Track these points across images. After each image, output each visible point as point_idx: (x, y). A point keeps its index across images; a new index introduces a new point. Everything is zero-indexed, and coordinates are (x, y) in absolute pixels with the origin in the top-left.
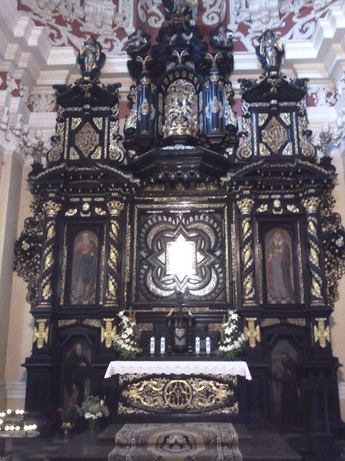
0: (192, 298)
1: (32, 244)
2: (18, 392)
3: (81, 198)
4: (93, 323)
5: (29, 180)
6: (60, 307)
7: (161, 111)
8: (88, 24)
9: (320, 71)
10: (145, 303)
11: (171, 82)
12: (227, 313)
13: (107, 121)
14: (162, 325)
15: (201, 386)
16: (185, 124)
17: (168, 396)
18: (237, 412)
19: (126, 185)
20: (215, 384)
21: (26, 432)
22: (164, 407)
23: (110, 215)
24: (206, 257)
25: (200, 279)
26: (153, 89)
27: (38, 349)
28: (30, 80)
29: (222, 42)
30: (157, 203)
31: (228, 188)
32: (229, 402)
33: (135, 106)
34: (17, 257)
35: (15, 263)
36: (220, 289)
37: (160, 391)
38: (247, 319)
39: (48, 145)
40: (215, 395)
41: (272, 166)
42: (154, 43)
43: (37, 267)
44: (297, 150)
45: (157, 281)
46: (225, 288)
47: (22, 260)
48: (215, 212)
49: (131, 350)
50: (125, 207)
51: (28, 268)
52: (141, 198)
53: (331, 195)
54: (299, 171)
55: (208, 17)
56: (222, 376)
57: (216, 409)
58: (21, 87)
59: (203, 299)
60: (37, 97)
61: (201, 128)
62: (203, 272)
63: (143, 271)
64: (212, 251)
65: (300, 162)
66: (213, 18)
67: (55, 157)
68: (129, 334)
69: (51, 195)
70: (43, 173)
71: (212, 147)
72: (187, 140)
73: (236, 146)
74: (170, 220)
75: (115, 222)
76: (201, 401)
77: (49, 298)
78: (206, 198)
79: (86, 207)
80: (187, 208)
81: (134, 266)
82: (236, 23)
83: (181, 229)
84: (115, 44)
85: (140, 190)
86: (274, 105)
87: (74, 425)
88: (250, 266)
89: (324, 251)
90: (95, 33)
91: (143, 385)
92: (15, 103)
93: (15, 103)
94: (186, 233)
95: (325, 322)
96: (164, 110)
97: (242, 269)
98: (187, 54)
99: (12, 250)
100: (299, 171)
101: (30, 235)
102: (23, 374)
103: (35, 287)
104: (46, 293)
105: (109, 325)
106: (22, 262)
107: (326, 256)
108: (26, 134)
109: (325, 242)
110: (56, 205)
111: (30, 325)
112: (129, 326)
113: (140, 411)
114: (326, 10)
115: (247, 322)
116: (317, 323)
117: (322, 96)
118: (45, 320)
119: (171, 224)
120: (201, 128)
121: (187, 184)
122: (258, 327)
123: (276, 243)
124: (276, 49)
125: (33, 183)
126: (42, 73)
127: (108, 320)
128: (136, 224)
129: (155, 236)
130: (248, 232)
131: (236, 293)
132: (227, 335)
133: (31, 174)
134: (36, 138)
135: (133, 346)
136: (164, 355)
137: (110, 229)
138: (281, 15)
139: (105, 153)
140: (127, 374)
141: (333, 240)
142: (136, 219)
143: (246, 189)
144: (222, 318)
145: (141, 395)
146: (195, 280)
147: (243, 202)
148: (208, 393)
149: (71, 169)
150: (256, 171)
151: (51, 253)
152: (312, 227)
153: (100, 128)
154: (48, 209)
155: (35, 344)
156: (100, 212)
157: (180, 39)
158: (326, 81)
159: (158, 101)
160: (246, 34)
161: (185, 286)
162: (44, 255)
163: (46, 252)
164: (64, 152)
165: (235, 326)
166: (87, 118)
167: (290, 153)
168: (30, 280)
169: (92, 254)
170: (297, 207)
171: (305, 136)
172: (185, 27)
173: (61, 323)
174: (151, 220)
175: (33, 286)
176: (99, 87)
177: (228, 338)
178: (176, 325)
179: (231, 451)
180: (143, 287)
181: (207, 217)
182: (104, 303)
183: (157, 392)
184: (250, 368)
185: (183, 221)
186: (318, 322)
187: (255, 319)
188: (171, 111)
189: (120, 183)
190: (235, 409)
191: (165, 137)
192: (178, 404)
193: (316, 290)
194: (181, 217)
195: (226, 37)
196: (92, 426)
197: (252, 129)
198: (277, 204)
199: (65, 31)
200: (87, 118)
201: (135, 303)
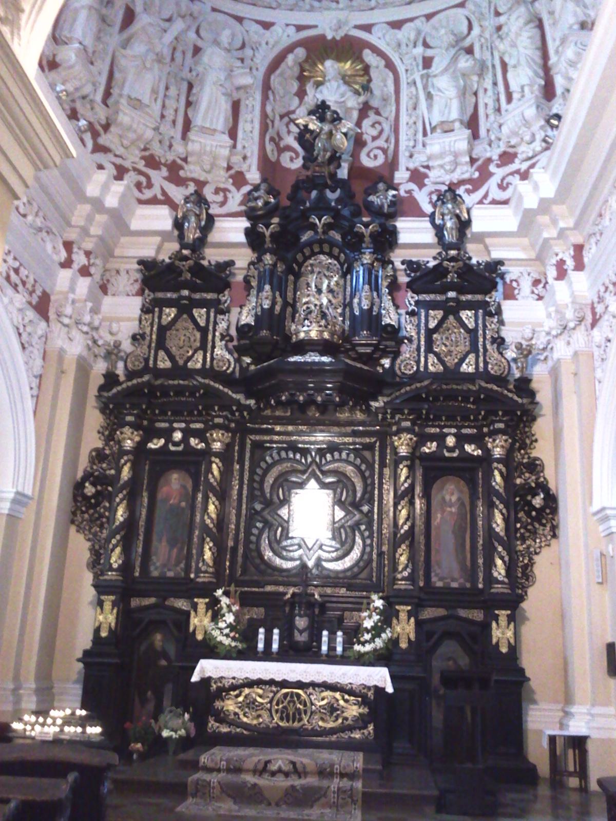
0: (325, 572)
1: (99, 488)
2: (70, 698)
3: (171, 422)
4: (180, 604)
5: (99, 397)
6: (134, 578)
7: (291, 301)
8: (191, 167)
9: (524, 249)
10: (255, 578)
11: (306, 258)
12: (369, 598)
13: (212, 314)
14: (277, 612)
15: (323, 699)
16: (323, 323)
17: (277, 711)
18: (372, 737)
19: (234, 408)
20: (343, 697)
21: (89, 736)
22: (271, 726)
23: (211, 449)
24: (348, 513)
25: (338, 546)
26: (280, 269)
27: (101, 638)
28: (106, 250)
29: (382, 207)
30: (279, 434)
31: (380, 416)
32: (361, 722)
33: (254, 292)
34: (76, 505)
35: (74, 513)
36: (364, 563)
37: (267, 703)
38: (397, 607)
39: (127, 346)
40: (343, 712)
41: (444, 387)
42: (286, 203)
43: (104, 520)
44: (481, 365)
45: (275, 546)
46: (370, 561)
47: (84, 509)
48: (363, 449)
49: (230, 645)
50: (233, 438)
51: (92, 521)
52: (257, 426)
53: (530, 431)
54: (482, 396)
55: (368, 155)
56: (354, 686)
57: (343, 732)
58: (92, 261)
59: (341, 575)
60: (114, 273)
61: (347, 328)
62: (343, 535)
63: (255, 531)
64: (356, 503)
65: (483, 384)
66: (376, 157)
67: (137, 363)
68: (228, 622)
69: (129, 418)
70: (119, 388)
71: (361, 358)
72: (324, 347)
73: (396, 354)
74: (298, 456)
75: (217, 460)
76: (322, 719)
77: (119, 566)
78: (349, 429)
79: (178, 436)
80: (322, 442)
81: (242, 524)
82: (408, 169)
83: (313, 470)
84: (229, 195)
85: (256, 415)
86: (452, 299)
87: (146, 747)
88: (406, 531)
89: (516, 513)
90: (202, 179)
91: (244, 694)
92: (83, 285)
93: (83, 285)
94: (321, 476)
95: (508, 616)
96: (295, 300)
97: (395, 534)
98: (330, 220)
99: (69, 495)
100: (482, 396)
101: (96, 473)
102: (79, 673)
103: (100, 548)
104: (116, 559)
105: (202, 607)
106: (83, 512)
107: (518, 520)
108: (97, 329)
109: (517, 499)
110: (136, 433)
111: (91, 603)
112: (230, 611)
113: (238, 730)
114: (534, 161)
115: (398, 611)
116: (496, 618)
117: (526, 286)
118: (112, 598)
119: (299, 462)
120: (347, 328)
121: (323, 408)
122: (412, 620)
123: (447, 498)
124: (458, 217)
125: (104, 400)
126: (124, 240)
127: (201, 600)
128: (247, 464)
129: (276, 480)
130: (405, 481)
131: (386, 569)
132: (366, 628)
133: (102, 388)
134: (111, 333)
135: (234, 639)
136: (278, 653)
137: (209, 470)
138: (473, 161)
139: (208, 359)
140: (222, 678)
141: (529, 498)
142: (248, 455)
143: (406, 420)
144: (361, 605)
145: (240, 707)
146: (331, 546)
147: (400, 439)
148: (332, 709)
149: (159, 382)
150: (420, 396)
151: (125, 502)
152: (498, 478)
153: (202, 323)
154: (124, 439)
155: (97, 631)
156: (197, 445)
157: (322, 198)
158: (532, 263)
159: (286, 287)
160: (421, 185)
161: (316, 555)
162: (115, 504)
163: (118, 500)
164: (149, 356)
165: (378, 617)
166: (185, 309)
167: (471, 370)
168: (94, 539)
169: (183, 504)
170: (479, 447)
171: (495, 345)
172: (329, 182)
173: (135, 602)
174: (271, 456)
175: (97, 547)
176: (203, 266)
177: (368, 633)
178: (297, 612)
179: (350, 783)
180: (254, 554)
181: (352, 455)
182: (197, 576)
183: (262, 704)
184: (393, 677)
185: (318, 460)
186: (498, 615)
187: (409, 608)
188: (304, 300)
189: (226, 404)
190: (369, 733)
191: (294, 340)
192: (291, 722)
193: (500, 569)
194: (313, 454)
195: (386, 198)
196: (171, 748)
197: (418, 333)
198: (451, 441)
199: (158, 177)
200: (185, 309)
201: (242, 578)
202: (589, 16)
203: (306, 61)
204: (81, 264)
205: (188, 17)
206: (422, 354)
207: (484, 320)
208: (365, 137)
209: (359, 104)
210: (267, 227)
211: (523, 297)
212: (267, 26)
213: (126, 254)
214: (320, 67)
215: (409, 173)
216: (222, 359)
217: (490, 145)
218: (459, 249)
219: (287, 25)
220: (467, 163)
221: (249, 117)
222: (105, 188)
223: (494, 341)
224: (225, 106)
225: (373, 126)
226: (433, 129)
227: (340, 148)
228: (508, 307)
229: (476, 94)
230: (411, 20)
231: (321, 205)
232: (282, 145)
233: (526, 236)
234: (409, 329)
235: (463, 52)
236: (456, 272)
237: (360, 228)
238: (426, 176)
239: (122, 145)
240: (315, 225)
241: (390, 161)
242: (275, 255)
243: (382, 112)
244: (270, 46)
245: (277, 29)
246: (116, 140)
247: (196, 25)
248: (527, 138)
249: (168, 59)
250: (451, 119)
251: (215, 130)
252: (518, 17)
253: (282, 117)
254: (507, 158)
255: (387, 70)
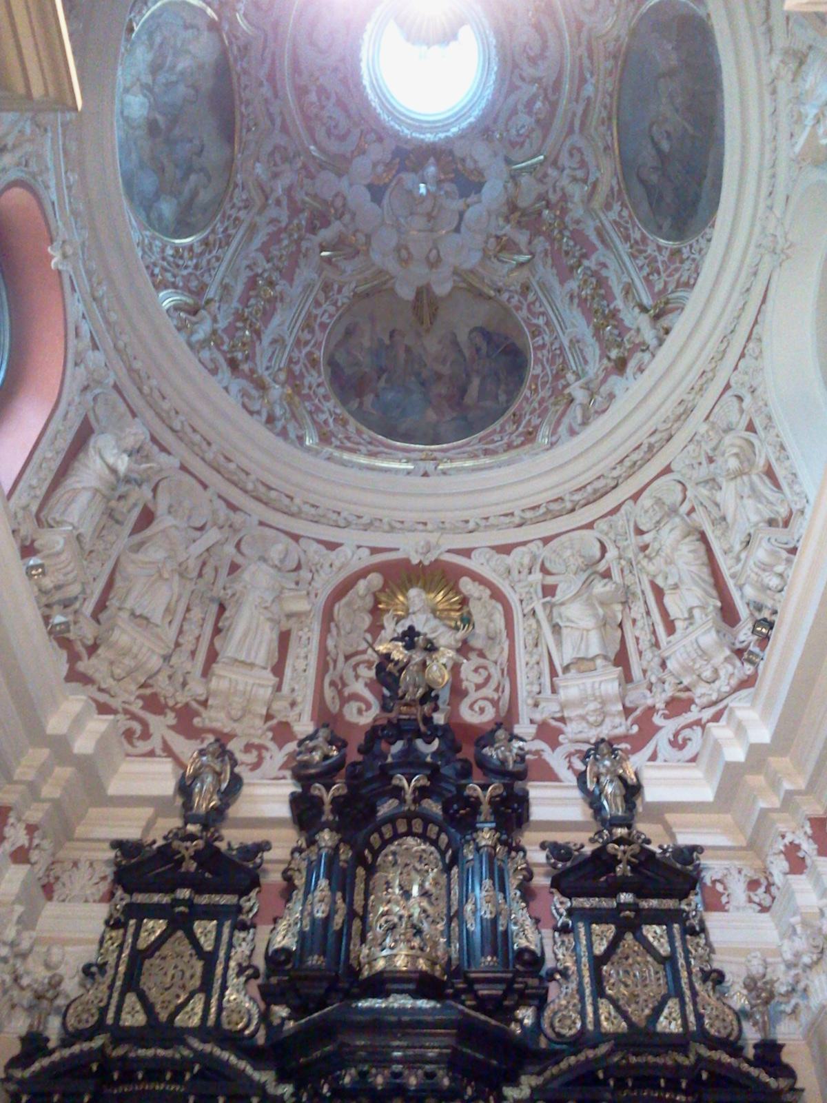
7: (360, 911)
11: (385, 843)
26: (343, 857)
28: (62, 825)
29: (503, 762)
33: (298, 895)
39: (71, 986)
41: (633, 1060)
44: (692, 1018)
54: (705, 1076)
55: (471, 707)
58: (36, 841)
60: (68, 865)
61: (455, 956)
66: (482, 710)
67: (85, 1016)
70: (45, 1062)
72: (424, 985)
73: (541, 1002)
82: (532, 722)
84: (266, 755)
90: (226, 730)
98: (424, 782)
108: (24, 956)
114: (721, 706)
117: (737, 890)
120: (455, 956)
124: (622, 779)
126: (93, 812)
134: (48, 966)
138: (627, 711)
139: (213, 1010)
149: (120, 1051)
150: (593, 1073)
157: (410, 750)
160: (554, 744)
164: (108, 1004)
166: (181, 922)
167: (675, 1027)
171: (710, 984)
172: (423, 728)
176: (218, 850)
195: (510, 751)
197: (578, 962)
199: (160, 725)
200: (181, 922)
202: (778, 513)
203: (382, 590)
204: (19, 844)
205: (226, 527)
206: (589, 1000)
207: (684, 942)
208: (465, 684)
209: (457, 641)
210: (328, 788)
211: (738, 908)
212: (332, 546)
213: (91, 836)
214: (401, 598)
215: (535, 726)
216: (238, 1010)
217: (650, 690)
218: (629, 827)
219: (359, 547)
220: (619, 713)
221: (302, 652)
222: (78, 722)
223: (706, 976)
224: (267, 638)
225: (476, 670)
226: (566, 669)
227: (438, 684)
228: (714, 921)
229: (620, 625)
230: (524, 544)
231: (411, 759)
232: (346, 694)
233: (726, 812)
234: (556, 953)
235: (598, 577)
236: (629, 863)
237: (473, 788)
238: (561, 732)
239: (112, 676)
240: (401, 789)
241: (503, 714)
242: (338, 832)
243: (487, 653)
244: (334, 569)
245: (347, 551)
246: (104, 668)
247: (237, 539)
248: (707, 674)
249: (195, 574)
250: (591, 655)
251: (252, 665)
252: (672, 530)
253: (347, 658)
254: (677, 706)
255: (493, 602)
